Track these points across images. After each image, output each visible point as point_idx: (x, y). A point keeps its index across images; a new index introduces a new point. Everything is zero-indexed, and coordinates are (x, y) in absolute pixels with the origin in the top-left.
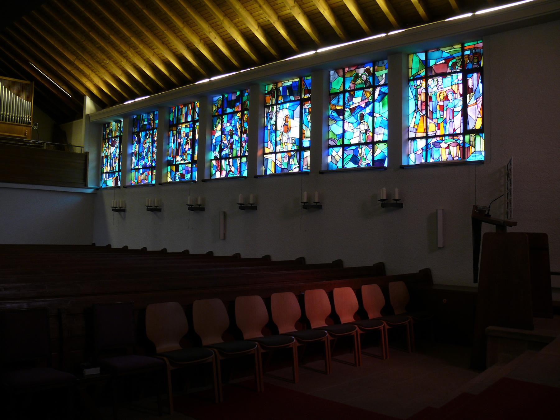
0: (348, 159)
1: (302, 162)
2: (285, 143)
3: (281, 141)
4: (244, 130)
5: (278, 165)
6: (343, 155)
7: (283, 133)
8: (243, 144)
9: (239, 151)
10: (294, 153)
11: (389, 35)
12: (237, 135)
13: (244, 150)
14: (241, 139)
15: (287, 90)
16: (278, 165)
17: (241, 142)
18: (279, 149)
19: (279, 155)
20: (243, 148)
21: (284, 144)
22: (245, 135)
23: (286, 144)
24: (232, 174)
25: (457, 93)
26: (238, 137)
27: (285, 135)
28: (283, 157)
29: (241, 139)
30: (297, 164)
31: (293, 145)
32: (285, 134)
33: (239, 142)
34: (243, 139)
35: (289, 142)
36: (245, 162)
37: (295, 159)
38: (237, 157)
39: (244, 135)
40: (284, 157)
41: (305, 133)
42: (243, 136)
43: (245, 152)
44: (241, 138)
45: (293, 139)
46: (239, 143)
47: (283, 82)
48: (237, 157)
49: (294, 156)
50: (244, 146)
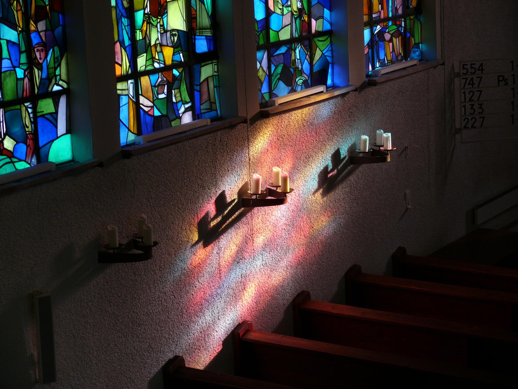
0: (277, 76)
1: (197, 94)
2: (155, 45)
3: (148, 42)
4: (36, 6)
5: (144, 111)
6: (269, 68)
7: (149, 18)
8: (38, 54)
9: (26, 80)
10: (180, 71)
11: (211, 13)
12: (13, 26)
13: (44, 76)
14: (28, 41)
15: (141, 252)
16: (147, 109)
17: (30, 50)
18: (141, 62)
19: (145, 81)
20: (40, 69)
21: (153, 49)
22: (42, 26)
23: (158, 49)
24: (8, 160)
25: (214, 87)
26: (15, 33)
27: (155, 24)
28: (155, 86)
29: (28, 41)
30: (188, 100)
31: (176, 50)
32: (154, 21)
33: (23, 48)
34: (35, 40)
35: (164, 43)
36: (51, 114)
37: (184, 87)
38: (19, 101)
39: (36, 24)
40: (159, 85)
41: (196, 18)
42: (33, 28)
43: (47, 81)
44: (26, 33)
45: (174, 33)
46: (21, 53)
47: (140, 93)
48: (19, 101)
49: (181, 80)
50: (41, 61)
